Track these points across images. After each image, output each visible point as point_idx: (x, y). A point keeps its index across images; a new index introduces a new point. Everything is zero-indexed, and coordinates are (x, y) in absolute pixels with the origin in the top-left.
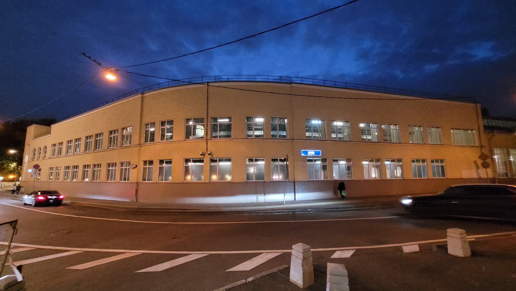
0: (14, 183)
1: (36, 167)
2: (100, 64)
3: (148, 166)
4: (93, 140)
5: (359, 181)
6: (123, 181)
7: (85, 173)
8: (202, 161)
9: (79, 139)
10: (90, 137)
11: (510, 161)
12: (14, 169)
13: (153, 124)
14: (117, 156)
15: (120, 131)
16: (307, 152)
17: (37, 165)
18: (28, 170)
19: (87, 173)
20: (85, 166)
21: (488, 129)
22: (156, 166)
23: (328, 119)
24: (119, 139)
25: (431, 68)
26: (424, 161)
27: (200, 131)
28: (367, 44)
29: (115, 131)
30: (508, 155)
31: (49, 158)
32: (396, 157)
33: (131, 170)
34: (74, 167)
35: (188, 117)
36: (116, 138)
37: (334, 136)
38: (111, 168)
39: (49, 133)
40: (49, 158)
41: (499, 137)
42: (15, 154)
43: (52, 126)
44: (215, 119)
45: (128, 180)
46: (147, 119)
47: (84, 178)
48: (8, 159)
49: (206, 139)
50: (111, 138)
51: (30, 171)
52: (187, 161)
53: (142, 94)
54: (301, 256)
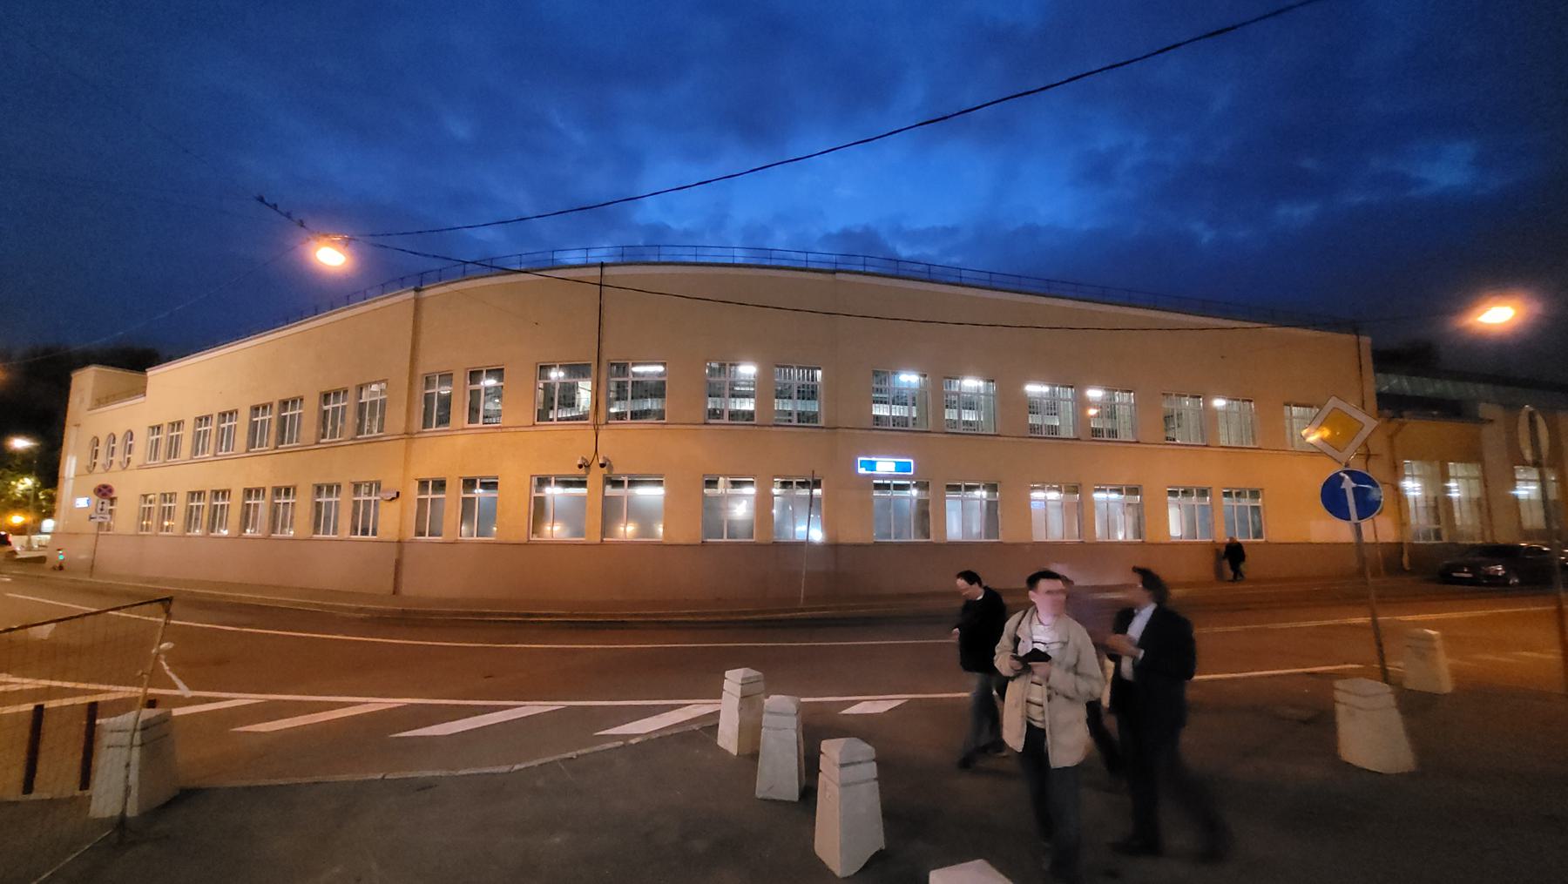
0: (25, 538)
1: (104, 492)
2: (302, 224)
3: (430, 495)
4: (271, 417)
5: (1014, 545)
6: (359, 537)
7: (247, 514)
8: (582, 484)
9: (231, 414)
10: (265, 407)
11: (1449, 501)
12: (25, 496)
13: (447, 378)
14: (343, 465)
15: (352, 394)
16: (873, 463)
17: (105, 487)
18: (75, 498)
19: (256, 511)
20: (248, 493)
21: (1391, 405)
22: (453, 496)
23: (941, 373)
24: (351, 417)
25: (1297, 213)
26: (1203, 493)
27: (584, 394)
28: (1106, 139)
29: (337, 394)
30: (1445, 477)
31: (140, 467)
32: (1123, 481)
33: (383, 506)
34: (217, 493)
35: (544, 361)
36: (341, 414)
37: (951, 414)
38: (323, 499)
39: (141, 391)
40: (140, 467)
41: (1418, 429)
42: (30, 451)
43: (151, 373)
44: (623, 368)
45: (374, 533)
46: (428, 364)
47: (244, 526)
48: (9, 467)
49: (597, 418)
50: (326, 412)
51: (82, 502)
52: (543, 482)
53: (417, 290)
54: (738, 691)
